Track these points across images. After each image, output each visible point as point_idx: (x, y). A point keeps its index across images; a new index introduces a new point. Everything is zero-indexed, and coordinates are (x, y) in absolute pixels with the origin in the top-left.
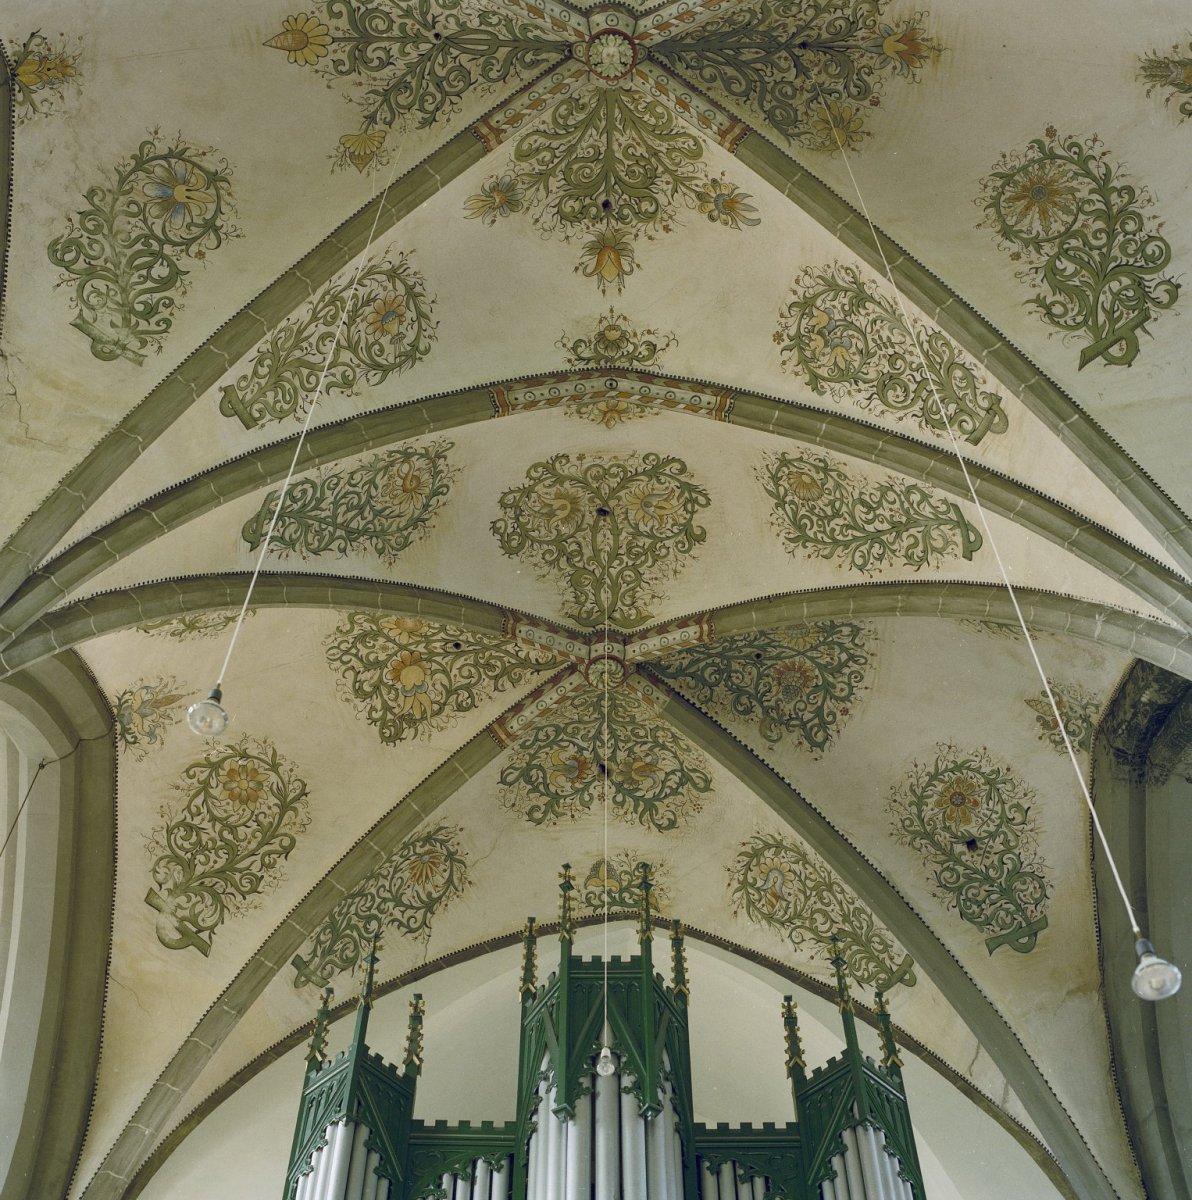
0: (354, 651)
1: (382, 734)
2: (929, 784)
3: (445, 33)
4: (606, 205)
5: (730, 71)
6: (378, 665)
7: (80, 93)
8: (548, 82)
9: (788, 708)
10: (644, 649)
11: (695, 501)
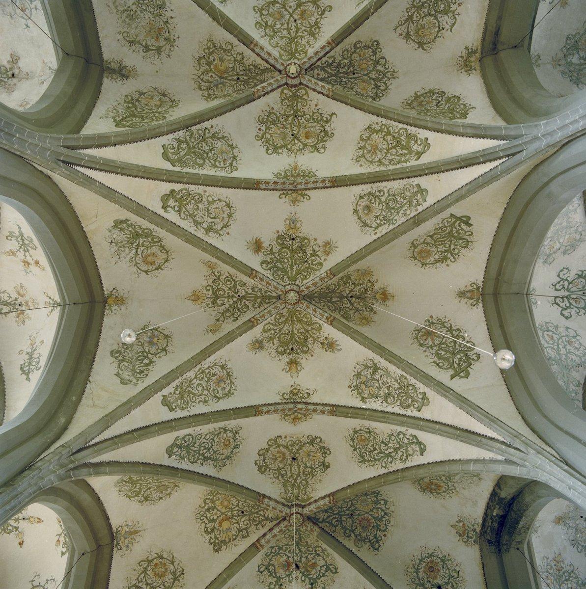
0: (205, 515)
1: (214, 548)
2: (420, 564)
3: (241, 295)
4: (292, 349)
5: (329, 304)
6: (214, 520)
9: (364, 535)
10: (310, 509)
11: (325, 453)
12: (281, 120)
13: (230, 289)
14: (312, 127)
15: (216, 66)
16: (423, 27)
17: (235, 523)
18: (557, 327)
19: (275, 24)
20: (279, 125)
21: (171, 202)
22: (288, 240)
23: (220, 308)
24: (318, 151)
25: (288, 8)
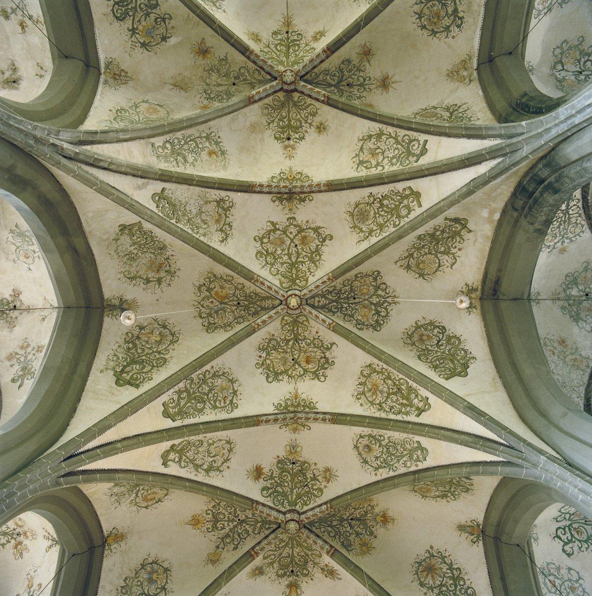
3: (241, 519)
5: (330, 529)
7: (126, 544)
8: (272, 536)
12: (282, 344)
13: (230, 513)
14: (313, 352)
16: (423, 262)
18: (558, 569)
19: (276, 250)
20: (280, 350)
21: (172, 456)
22: (289, 464)
23: (220, 532)
24: (319, 379)
25: (288, 234)
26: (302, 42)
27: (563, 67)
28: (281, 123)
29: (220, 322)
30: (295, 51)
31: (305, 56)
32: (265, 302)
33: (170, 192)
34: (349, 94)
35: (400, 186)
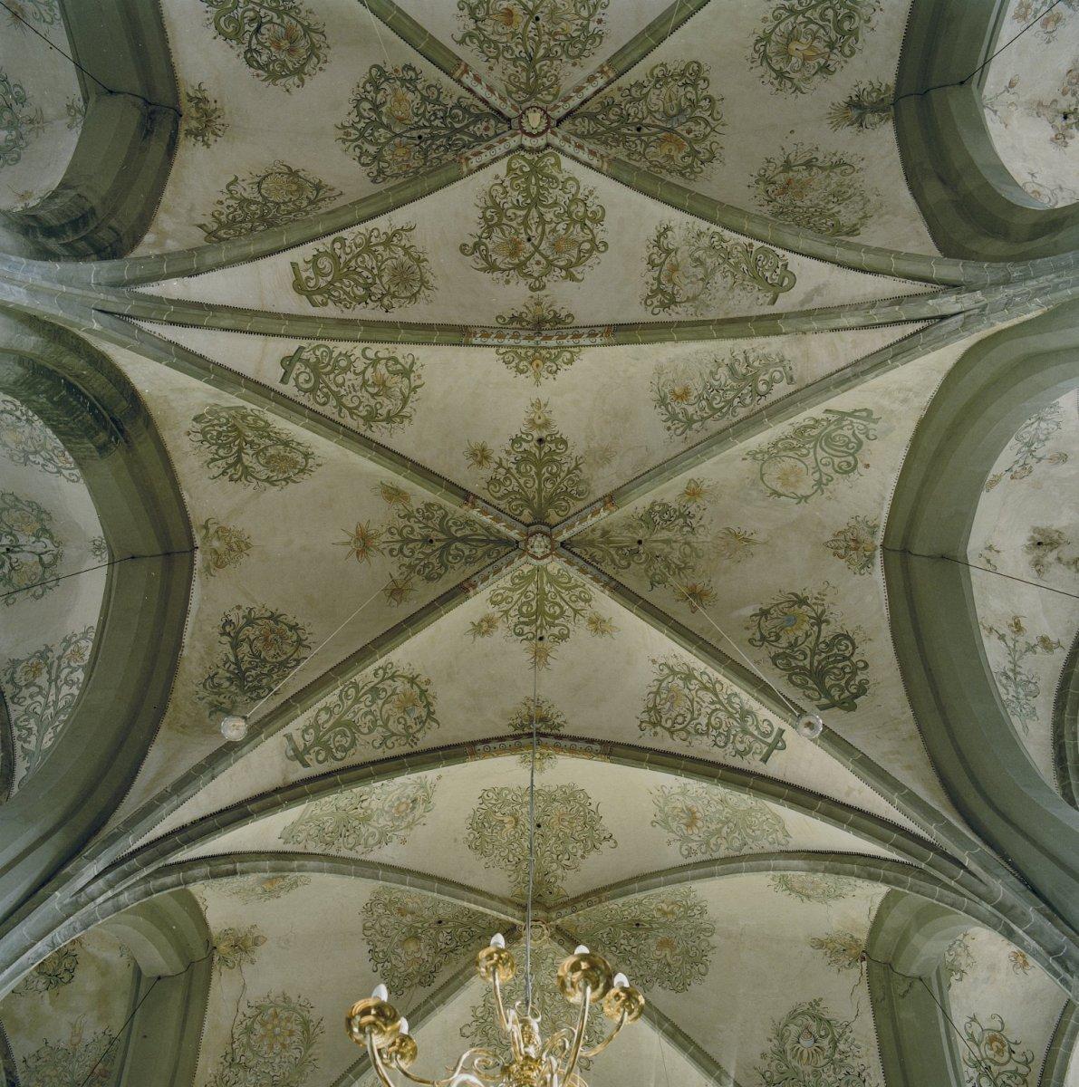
12: (558, 49)
15: (680, 150)
17: (655, 112)
19: (566, 230)
20: (563, 38)
25: (543, 261)
26: (515, 620)
27: (41, 559)
28: (555, 470)
29: (674, 90)
30: (528, 603)
31: (510, 590)
32: (588, 130)
33: (761, 301)
34: (430, 524)
35: (332, 311)
